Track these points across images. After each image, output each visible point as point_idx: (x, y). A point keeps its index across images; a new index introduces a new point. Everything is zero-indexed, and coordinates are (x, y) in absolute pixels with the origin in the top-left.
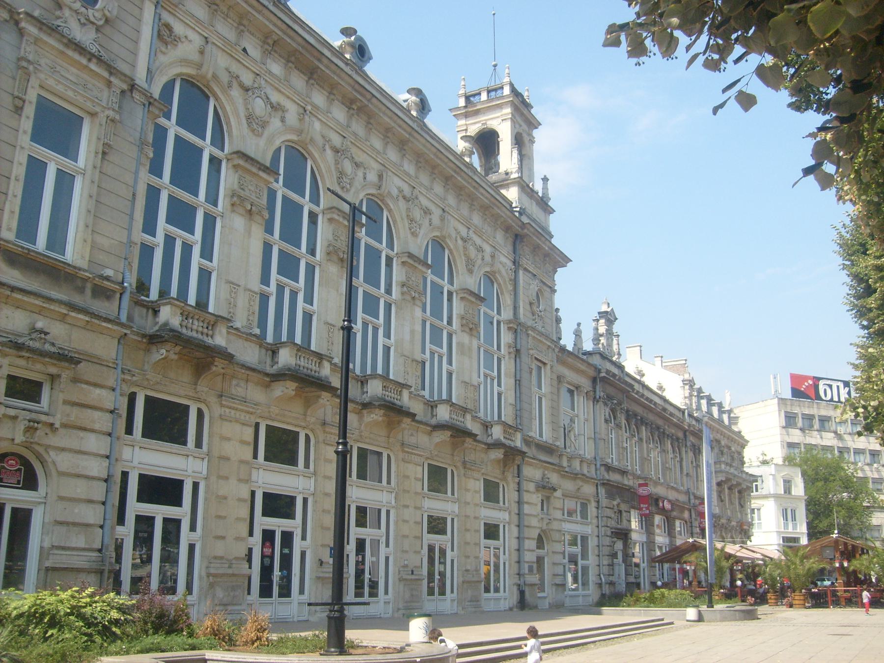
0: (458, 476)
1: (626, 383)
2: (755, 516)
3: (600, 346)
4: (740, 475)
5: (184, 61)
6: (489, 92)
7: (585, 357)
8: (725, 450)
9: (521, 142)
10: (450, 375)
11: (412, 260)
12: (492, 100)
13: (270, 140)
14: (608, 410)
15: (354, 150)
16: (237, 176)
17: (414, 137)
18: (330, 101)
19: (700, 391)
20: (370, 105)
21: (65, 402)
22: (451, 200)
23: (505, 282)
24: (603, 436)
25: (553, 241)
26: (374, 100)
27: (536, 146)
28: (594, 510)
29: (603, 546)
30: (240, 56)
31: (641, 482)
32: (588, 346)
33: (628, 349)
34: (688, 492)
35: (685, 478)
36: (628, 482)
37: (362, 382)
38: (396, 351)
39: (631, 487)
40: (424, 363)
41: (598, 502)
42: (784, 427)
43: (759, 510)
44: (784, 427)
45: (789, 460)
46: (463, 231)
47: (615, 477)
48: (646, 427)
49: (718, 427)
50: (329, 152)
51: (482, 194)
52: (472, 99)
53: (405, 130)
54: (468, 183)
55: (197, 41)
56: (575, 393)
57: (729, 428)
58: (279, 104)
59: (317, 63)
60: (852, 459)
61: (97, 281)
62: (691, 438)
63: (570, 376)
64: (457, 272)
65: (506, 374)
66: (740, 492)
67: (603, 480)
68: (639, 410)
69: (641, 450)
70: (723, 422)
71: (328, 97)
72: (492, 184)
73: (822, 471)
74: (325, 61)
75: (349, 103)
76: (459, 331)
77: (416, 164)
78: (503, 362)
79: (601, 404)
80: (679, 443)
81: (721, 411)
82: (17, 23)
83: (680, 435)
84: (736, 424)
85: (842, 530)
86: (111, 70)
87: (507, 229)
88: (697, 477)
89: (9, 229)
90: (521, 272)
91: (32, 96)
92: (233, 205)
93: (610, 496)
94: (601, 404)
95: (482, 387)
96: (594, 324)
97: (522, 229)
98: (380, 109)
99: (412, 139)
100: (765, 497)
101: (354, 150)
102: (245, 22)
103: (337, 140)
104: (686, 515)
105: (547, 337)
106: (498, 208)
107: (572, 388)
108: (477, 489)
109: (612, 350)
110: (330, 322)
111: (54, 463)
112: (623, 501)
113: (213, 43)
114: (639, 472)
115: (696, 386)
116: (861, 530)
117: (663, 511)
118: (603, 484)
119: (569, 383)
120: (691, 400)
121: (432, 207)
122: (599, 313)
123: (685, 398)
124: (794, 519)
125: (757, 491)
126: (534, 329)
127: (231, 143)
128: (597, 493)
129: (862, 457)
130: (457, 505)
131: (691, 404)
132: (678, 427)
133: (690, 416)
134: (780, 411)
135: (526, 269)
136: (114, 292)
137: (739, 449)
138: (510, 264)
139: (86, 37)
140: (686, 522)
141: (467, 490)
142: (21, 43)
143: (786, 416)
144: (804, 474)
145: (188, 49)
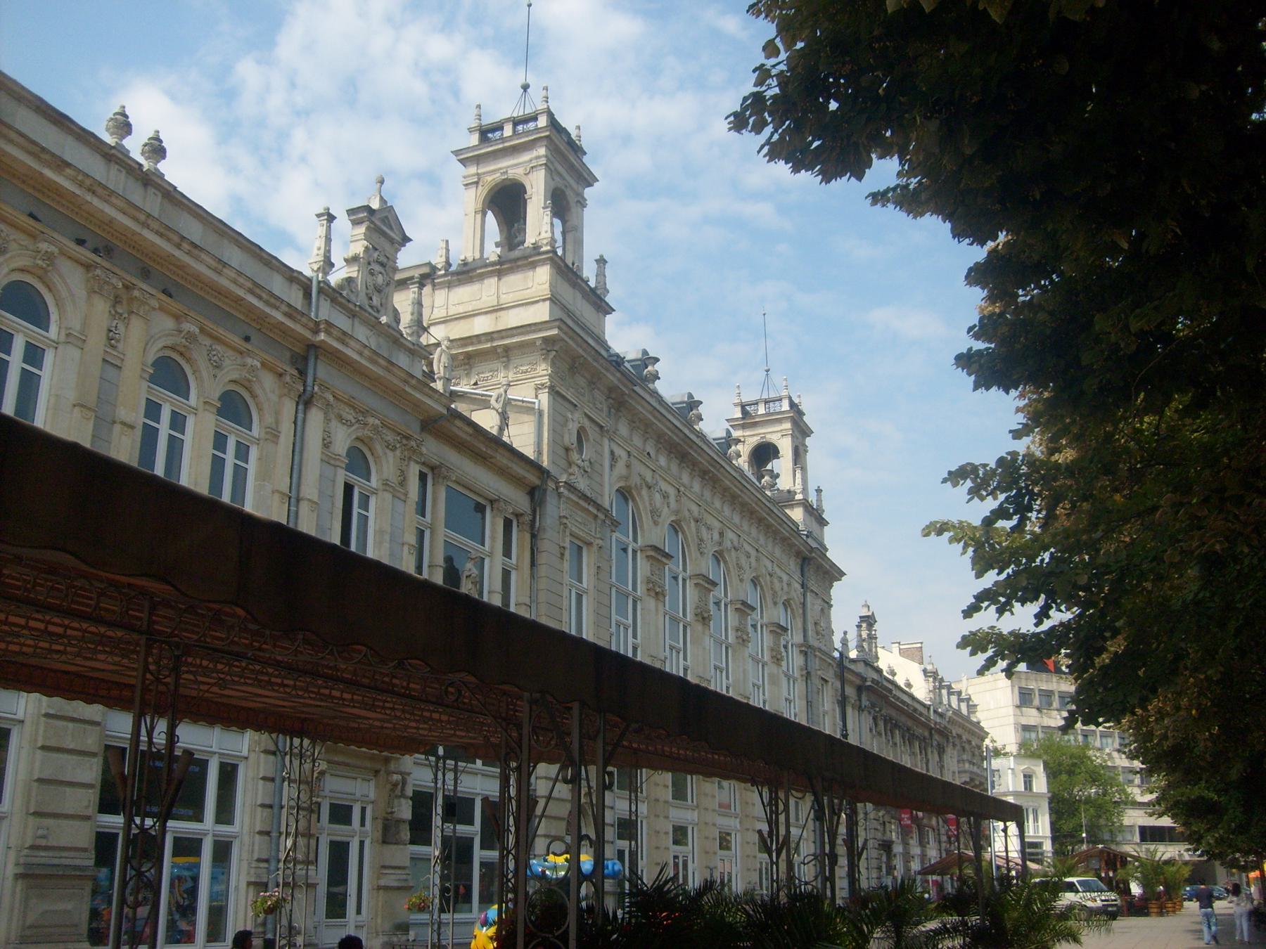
5: (621, 478)
8: (967, 747)
9: (799, 454)
16: (649, 564)
17: (745, 494)
19: (942, 680)
20: (608, 375)
25: (828, 554)
27: (809, 456)
29: (872, 858)
30: (646, 460)
32: (853, 654)
33: (352, 244)
42: (1017, 707)
44: (1017, 707)
52: (748, 408)
55: (623, 454)
57: (967, 719)
60: (1098, 744)
62: (936, 737)
65: (799, 697)
68: (893, 713)
71: (690, 474)
73: (1067, 761)
81: (960, 700)
82: (557, 488)
87: (798, 554)
90: (809, 596)
91: (567, 545)
92: (648, 590)
97: (811, 553)
102: (649, 430)
103: (695, 508)
107: (425, 470)
110: (653, 654)
113: (634, 456)
115: (940, 677)
122: (860, 617)
123: (930, 691)
126: (820, 650)
127: (643, 536)
129: (1110, 740)
130: (696, 813)
132: (925, 725)
134: (1013, 686)
135: (812, 591)
139: (582, 484)
140: (934, 829)
141: (706, 795)
142: (559, 504)
143: (1020, 693)
145: (620, 468)
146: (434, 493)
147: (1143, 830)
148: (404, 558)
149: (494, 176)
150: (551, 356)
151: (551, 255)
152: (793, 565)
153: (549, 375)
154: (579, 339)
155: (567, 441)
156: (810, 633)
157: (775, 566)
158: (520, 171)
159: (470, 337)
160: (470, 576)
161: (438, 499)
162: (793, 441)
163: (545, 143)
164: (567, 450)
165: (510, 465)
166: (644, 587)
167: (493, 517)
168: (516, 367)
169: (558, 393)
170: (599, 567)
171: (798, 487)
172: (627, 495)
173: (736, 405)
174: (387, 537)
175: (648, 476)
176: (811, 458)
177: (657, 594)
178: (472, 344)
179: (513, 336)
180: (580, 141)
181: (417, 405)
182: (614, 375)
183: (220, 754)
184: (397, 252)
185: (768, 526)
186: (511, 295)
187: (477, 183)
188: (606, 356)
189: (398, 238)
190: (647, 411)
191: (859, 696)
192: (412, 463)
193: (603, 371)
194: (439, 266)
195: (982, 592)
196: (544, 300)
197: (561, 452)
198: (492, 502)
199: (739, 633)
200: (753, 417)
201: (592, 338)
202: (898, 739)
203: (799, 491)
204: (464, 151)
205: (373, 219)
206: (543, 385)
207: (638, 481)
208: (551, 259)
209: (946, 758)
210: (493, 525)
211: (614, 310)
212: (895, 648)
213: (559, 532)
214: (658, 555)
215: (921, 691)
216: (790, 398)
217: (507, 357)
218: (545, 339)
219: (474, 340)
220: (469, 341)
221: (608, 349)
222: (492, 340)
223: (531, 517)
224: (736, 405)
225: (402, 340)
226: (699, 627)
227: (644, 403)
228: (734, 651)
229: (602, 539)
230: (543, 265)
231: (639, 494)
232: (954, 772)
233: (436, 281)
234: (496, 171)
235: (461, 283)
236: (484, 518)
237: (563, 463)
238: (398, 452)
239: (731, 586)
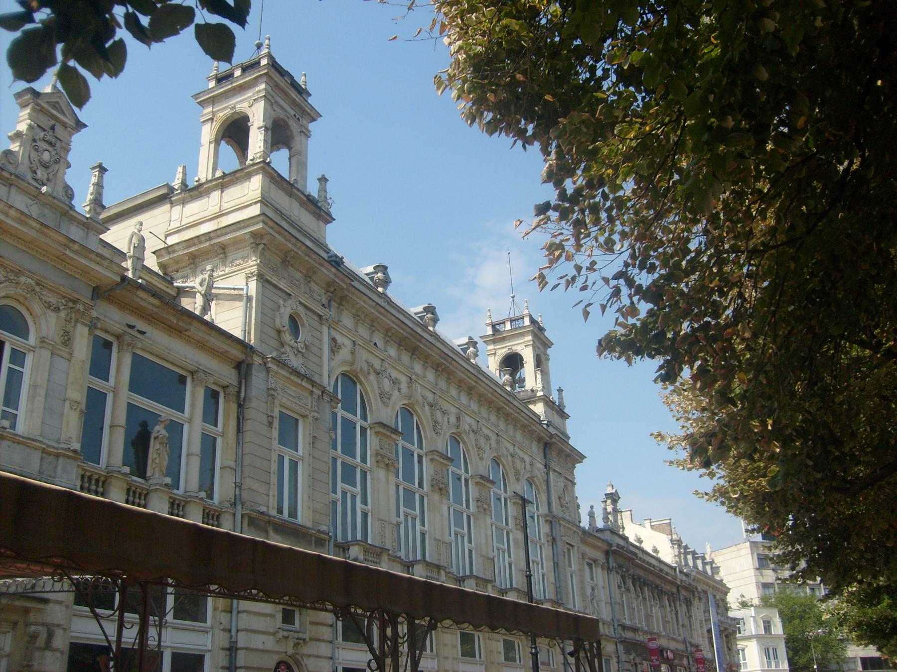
0: (522, 646)
1: (631, 552)
3: (609, 523)
4: (726, 621)
5: (344, 362)
6: (511, 321)
7: (599, 535)
9: (540, 362)
10: (510, 564)
12: (515, 329)
14: (619, 577)
15: (441, 402)
16: (378, 439)
17: (480, 385)
18: (425, 367)
19: (686, 547)
21: (312, 623)
22: (502, 425)
23: (541, 484)
24: (618, 600)
25: (571, 442)
26: (454, 362)
27: (550, 363)
28: (616, 664)
30: (373, 349)
31: (649, 637)
32: (600, 524)
34: (684, 641)
35: (681, 628)
36: (640, 637)
37: (344, 549)
38: (476, 552)
39: (642, 642)
40: (398, 525)
41: (618, 657)
42: (757, 569)
43: (743, 650)
44: (757, 569)
45: (766, 602)
46: (511, 448)
47: (629, 635)
49: (704, 579)
50: (427, 408)
51: (522, 417)
52: (497, 327)
53: (473, 380)
54: (513, 410)
55: (348, 343)
56: (593, 565)
57: (712, 578)
58: (396, 379)
59: (419, 344)
61: (318, 535)
62: (683, 592)
63: (592, 553)
64: (509, 482)
65: (546, 559)
66: (727, 636)
67: (621, 638)
68: (641, 573)
69: (645, 608)
70: (707, 574)
71: (423, 365)
72: (521, 401)
74: (424, 341)
75: (437, 367)
76: (514, 530)
77: (479, 403)
78: (543, 549)
79: (614, 572)
80: (674, 597)
82: (265, 364)
83: (674, 590)
84: (718, 573)
85: (820, 664)
86: (313, 383)
87: (539, 440)
88: (691, 627)
89: (273, 508)
90: (551, 473)
91: (276, 414)
92: (377, 462)
93: (628, 652)
94: (614, 572)
95: (496, 560)
96: (603, 505)
97: (551, 439)
98: (456, 368)
99: (477, 386)
100: (749, 638)
101: (441, 402)
103: (430, 396)
104: (685, 662)
105: (573, 524)
106: (534, 425)
107: (591, 562)
109: (618, 525)
111: (306, 665)
112: (638, 655)
114: (646, 628)
115: (683, 544)
116: (838, 663)
117: (667, 661)
118: (621, 642)
120: (680, 558)
122: (606, 495)
123: (675, 556)
124: (776, 657)
125: (740, 633)
126: (564, 519)
128: (617, 650)
131: (681, 562)
132: (673, 583)
133: (681, 572)
134: (752, 553)
135: (555, 471)
136: (325, 540)
137: (722, 597)
138: (542, 467)
139: (296, 362)
142: (268, 378)
144: (781, 614)
145: (344, 353)
146: (596, 573)
148: (65, 413)
149: (226, 112)
151: (261, 165)
152: (535, 449)
153: (258, 265)
154: (287, 234)
155: (278, 324)
156: (554, 505)
157: (516, 448)
158: (246, 105)
160: (158, 437)
162: (534, 351)
163: (265, 79)
164: (279, 332)
165: (207, 337)
166: (374, 458)
167: (194, 387)
168: (231, 262)
169: (267, 281)
170: (314, 437)
171: (539, 386)
172: (354, 379)
173: (487, 325)
174: (42, 392)
175: (377, 364)
176: (552, 366)
177: (441, 489)
178: (194, 245)
179: (226, 234)
180: (305, 85)
181: (86, 272)
183: (171, 647)
185: (507, 415)
186: (231, 203)
187: (212, 119)
188: (326, 258)
189: (70, 122)
191: (607, 559)
192: (79, 326)
193: (317, 265)
194: (176, 187)
195: (234, 42)
196: (256, 203)
197: (273, 333)
198: (192, 373)
199: (480, 503)
200: (501, 333)
202: (647, 593)
203: (539, 389)
204: (202, 95)
205: (39, 101)
206: (251, 273)
209: (694, 610)
211: (334, 220)
212: (647, 523)
213: (267, 403)
214: (484, 481)
215: (668, 555)
216: (530, 316)
217: (224, 253)
218: (253, 234)
219: (196, 241)
220: (191, 242)
221: (328, 251)
222: (210, 239)
223: (236, 389)
224: (487, 325)
225: (71, 212)
226: (436, 497)
227: (365, 297)
228: (476, 519)
229: (318, 413)
230: (256, 175)
231: (366, 378)
232: (701, 621)
233: (172, 199)
234: (224, 111)
235: (193, 198)
236: (110, 355)
237: (275, 343)
238: (63, 314)
239: (471, 463)
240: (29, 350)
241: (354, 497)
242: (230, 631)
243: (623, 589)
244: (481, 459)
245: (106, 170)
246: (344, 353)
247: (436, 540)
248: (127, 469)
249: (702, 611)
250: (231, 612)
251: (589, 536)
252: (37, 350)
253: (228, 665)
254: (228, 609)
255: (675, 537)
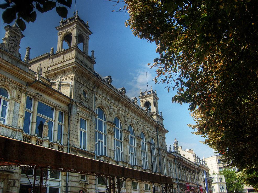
1: (182, 159)
2: (213, 188)
5: (99, 104)
6: (147, 92)
9: (155, 104)
11: (110, 123)
12: (148, 95)
13: (113, 117)
16: (124, 134)
21: (90, 179)
28: (177, 191)
32: (173, 150)
36: (184, 183)
39: (185, 184)
43: (214, 187)
45: (220, 173)
47: (181, 182)
48: (173, 164)
57: (205, 166)
66: (209, 183)
81: (203, 162)
83: (194, 169)
86: (90, 110)
87: (155, 126)
91: (79, 119)
93: (181, 187)
96: (173, 145)
100: (215, 183)
102: (108, 93)
103: (124, 114)
104: (197, 190)
108: (131, 185)
112: (183, 188)
117: (192, 190)
119: (169, 160)
120: (196, 160)
121: (141, 125)
124: (223, 189)
126: (162, 149)
127: (107, 119)
132: (194, 168)
135: (159, 135)
137: (208, 171)
138: (156, 134)
139: (85, 104)
141: (128, 185)
144: (225, 176)
145: (99, 102)
146: (56, 113)
147: (248, 190)
150: (75, 72)
153: (74, 76)
158: (71, 30)
159: (55, 68)
161: (35, 105)
162: (154, 101)
164: (80, 95)
165: (60, 97)
166: (107, 132)
168: (66, 75)
169: (77, 81)
170: (90, 125)
171: (155, 111)
174: (12, 113)
175: (108, 104)
176: (159, 105)
177: (127, 140)
179: (65, 67)
182: (95, 78)
184: (20, 39)
187: (61, 34)
189: (20, 35)
190: (106, 88)
191: (175, 161)
194: (51, 54)
196: (73, 58)
198: (55, 107)
201: (89, 69)
207: (105, 106)
208: (76, 48)
209: (200, 175)
210: (56, 114)
214: (139, 138)
215: (192, 159)
216: (153, 91)
217: (65, 73)
218: (73, 67)
220: (55, 70)
221: (94, 72)
222: (60, 69)
226: (125, 143)
228: (137, 149)
231: (105, 109)
232: (202, 178)
234: (64, 32)
235: (56, 57)
237: (79, 99)
238: (18, 90)
240: (8, 101)
241: (102, 143)
242: (66, 181)
243: (179, 169)
244: (138, 132)
245: (30, 49)
246: (99, 102)
247: (125, 155)
248: (37, 135)
249: (202, 175)
250: (66, 176)
251: (169, 154)
252: (11, 100)
253: (65, 191)
254: (66, 175)
255: (194, 154)
